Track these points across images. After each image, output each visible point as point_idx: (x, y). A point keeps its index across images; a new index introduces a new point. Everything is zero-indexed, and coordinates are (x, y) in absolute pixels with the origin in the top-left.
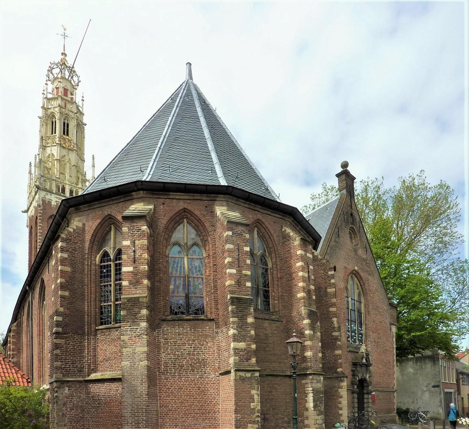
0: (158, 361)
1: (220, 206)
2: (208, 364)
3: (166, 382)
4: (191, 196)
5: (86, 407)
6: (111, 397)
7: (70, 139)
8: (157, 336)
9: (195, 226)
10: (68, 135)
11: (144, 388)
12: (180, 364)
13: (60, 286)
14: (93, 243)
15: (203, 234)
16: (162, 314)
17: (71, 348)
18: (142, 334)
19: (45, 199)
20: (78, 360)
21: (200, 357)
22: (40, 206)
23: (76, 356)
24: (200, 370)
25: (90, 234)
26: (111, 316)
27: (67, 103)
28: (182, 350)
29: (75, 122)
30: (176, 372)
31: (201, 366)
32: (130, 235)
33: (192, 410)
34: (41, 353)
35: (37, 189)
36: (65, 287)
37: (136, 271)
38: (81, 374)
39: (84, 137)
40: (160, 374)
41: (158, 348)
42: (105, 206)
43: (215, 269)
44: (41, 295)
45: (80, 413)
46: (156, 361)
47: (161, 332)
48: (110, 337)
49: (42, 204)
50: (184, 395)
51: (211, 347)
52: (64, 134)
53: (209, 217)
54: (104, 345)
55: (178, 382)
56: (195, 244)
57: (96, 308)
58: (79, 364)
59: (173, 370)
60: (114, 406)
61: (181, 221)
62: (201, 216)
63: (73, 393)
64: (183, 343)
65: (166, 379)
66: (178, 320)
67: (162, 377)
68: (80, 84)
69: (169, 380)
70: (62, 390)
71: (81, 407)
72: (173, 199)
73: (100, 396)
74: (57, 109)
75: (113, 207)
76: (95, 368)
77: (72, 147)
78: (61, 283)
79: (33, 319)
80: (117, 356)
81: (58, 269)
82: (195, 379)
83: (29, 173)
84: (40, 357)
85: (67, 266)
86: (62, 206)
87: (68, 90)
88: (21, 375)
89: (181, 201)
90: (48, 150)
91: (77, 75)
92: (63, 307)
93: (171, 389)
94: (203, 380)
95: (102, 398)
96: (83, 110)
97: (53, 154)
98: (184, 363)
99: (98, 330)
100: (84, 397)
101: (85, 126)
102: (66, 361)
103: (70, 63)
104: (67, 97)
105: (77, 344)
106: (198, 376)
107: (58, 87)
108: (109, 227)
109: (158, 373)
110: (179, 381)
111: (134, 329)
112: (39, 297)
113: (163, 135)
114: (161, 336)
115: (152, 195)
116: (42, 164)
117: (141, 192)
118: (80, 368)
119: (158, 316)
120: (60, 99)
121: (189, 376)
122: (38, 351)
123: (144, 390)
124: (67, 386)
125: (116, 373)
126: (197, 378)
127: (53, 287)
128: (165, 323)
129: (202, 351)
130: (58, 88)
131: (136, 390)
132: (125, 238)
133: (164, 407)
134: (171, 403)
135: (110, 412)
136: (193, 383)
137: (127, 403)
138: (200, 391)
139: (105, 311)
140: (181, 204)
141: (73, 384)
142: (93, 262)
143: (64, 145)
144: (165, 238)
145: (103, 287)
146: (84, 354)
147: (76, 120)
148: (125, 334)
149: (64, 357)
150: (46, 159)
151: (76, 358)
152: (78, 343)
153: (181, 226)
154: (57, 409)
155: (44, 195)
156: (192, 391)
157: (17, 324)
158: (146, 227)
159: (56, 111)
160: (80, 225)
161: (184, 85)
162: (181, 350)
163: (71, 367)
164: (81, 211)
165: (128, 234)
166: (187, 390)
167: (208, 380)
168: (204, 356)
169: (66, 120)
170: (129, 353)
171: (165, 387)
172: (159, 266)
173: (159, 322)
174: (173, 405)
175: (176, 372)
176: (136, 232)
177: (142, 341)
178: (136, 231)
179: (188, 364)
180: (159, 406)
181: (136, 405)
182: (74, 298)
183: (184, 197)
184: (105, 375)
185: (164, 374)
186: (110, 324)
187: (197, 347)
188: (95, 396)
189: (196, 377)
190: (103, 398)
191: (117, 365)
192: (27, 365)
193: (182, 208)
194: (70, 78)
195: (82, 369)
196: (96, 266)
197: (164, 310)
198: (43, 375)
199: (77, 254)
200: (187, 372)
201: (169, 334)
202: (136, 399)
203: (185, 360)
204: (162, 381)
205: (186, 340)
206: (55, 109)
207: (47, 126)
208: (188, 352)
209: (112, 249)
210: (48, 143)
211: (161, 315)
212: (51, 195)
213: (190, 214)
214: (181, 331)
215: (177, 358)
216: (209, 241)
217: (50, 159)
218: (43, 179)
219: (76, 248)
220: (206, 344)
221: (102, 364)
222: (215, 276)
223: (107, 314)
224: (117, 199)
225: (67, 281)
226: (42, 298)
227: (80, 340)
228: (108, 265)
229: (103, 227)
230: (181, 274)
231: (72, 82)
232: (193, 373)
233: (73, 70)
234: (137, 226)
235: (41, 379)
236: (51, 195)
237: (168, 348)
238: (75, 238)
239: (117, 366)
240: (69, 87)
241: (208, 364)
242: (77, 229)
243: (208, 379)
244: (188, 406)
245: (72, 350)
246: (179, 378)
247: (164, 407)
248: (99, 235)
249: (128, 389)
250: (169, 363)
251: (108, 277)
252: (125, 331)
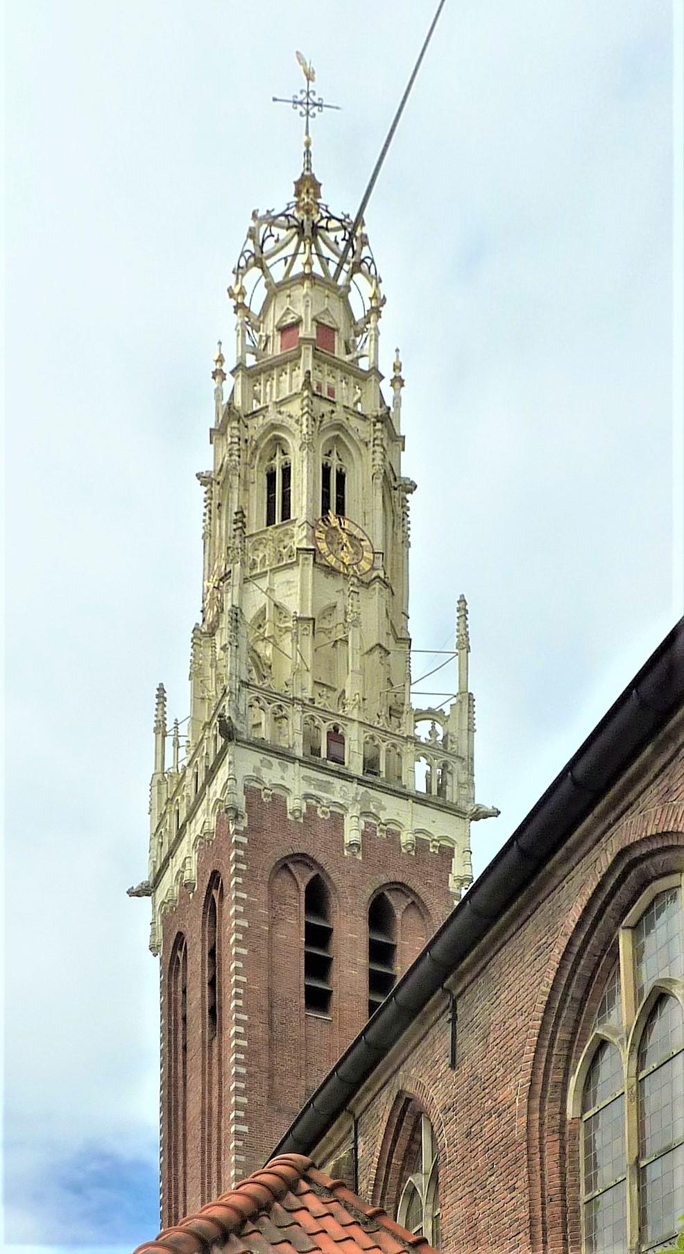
19: (258, 786)
22: (236, 817)
35: (221, 741)
49: (244, 805)
74: (295, 408)
83: (156, 730)
87: (333, 330)
101: (408, 496)
143: (332, 560)
155: (257, 770)
159: (290, 416)
206: (282, 409)
212: (284, 768)
233: (358, 234)
236: (284, 768)
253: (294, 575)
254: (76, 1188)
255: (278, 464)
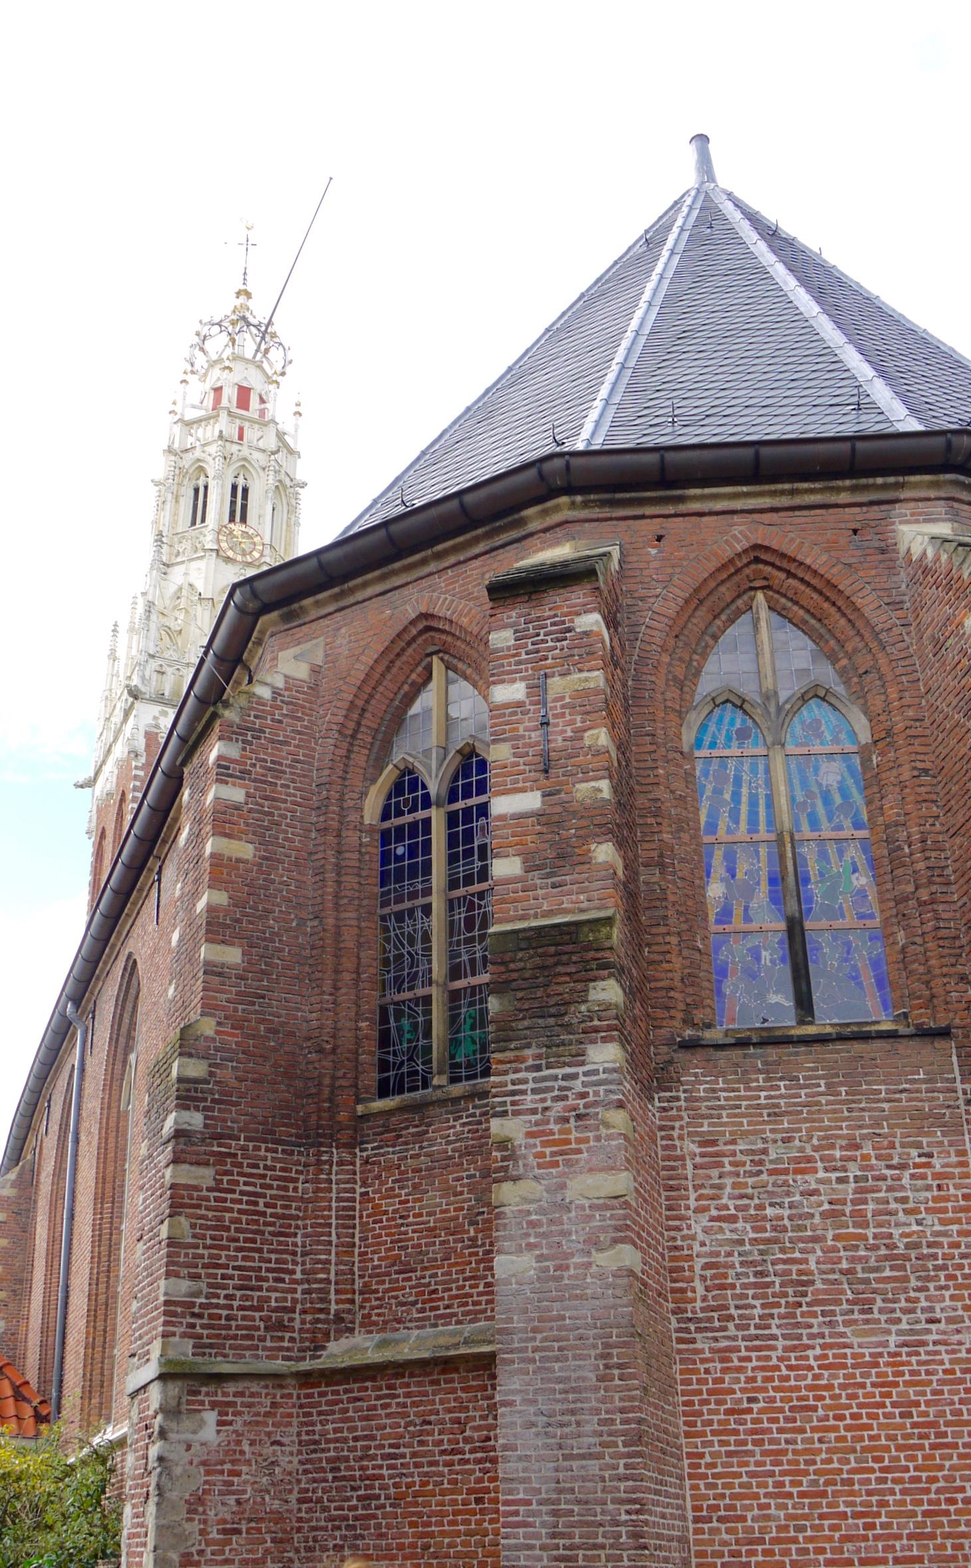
0: (673, 1259)
1: (917, 522)
2: (944, 1267)
3: (725, 1370)
4: (782, 493)
5: (300, 1520)
6: (431, 1464)
7: (251, 532)
8: (661, 1128)
9: (807, 617)
10: (244, 519)
11: (621, 1399)
12: (788, 1273)
13: (208, 923)
14: (353, 737)
15: (849, 647)
16: (680, 1015)
17: (240, 1211)
18: (595, 1104)
20: (268, 1270)
21: (896, 1232)
22: (137, 756)
23: (260, 1250)
24: (903, 1304)
25: (339, 704)
26: (428, 1049)
27: (245, 429)
28: (797, 1198)
29: (271, 477)
30: (772, 1316)
31: (906, 1279)
32: (524, 657)
33: (877, 1538)
34: (103, 1279)
35: (131, 699)
36: (228, 927)
37: (558, 809)
38: (282, 1339)
39: (297, 524)
40: (687, 1330)
41: (671, 1188)
42: (407, 584)
43: (928, 789)
44: (119, 1030)
45: (267, 1551)
46: (663, 1256)
47: (682, 1103)
48: (421, 1148)
49: (143, 747)
50: (828, 1450)
51: (950, 1176)
52: (232, 519)
53: (873, 572)
54: (392, 1189)
55: (785, 1372)
56: (815, 694)
57: (358, 1017)
58: (276, 1290)
59: (757, 1303)
60: (442, 1514)
61: (740, 602)
62: (834, 570)
63: (239, 1443)
64: (797, 1160)
65: (724, 1355)
66: (762, 1044)
67: (699, 1346)
68: (288, 369)
69: (736, 1363)
70: (187, 1423)
71: (278, 1518)
72: (701, 514)
73: (374, 1458)
74: (212, 449)
75: (440, 581)
76: (349, 1311)
77: (256, 555)
78: (210, 909)
79: (83, 1137)
80: (455, 1241)
81: (200, 856)
82: (881, 1355)
84: (97, 1295)
85: (240, 839)
86: (232, 610)
88: (12, 1384)
89: (736, 518)
90: (177, 576)
91: (280, 344)
92: (213, 1015)
93: (750, 1411)
94: (923, 1357)
95: (381, 1467)
96: (296, 442)
97: (191, 585)
98: (813, 1266)
99: (365, 1117)
100: (289, 1468)
102: (215, 1276)
103: (259, 311)
104: (247, 409)
105: (270, 1187)
106: (893, 1339)
107: (219, 385)
108: (420, 669)
109: (674, 1324)
110: (790, 1368)
111: (556, 1078)
112: (111, 1039)
113: (614, 362)
114: (681, 1128)
115: (607, 510)
116: (154, 617)
117: (564, 500)
118: (276, 1310)
119: (661, 1027)
120: (223, 416)
121: (843, 1335)
122: (92, 1269)
123: (622, 1411)
124: (214, 1405)
125: (453, 1334)
126: (892, 1349)
127: (175, 937)
128: (697, 1057)
129: (904, 1200)
130: (221, 388)
131: (573, 1412)
132: (504, 673)
133: (720, 1519)
134: (756, 1496)
135: (426, 1547)
136: (868, 1375)
137: (526, 1491)
138: (915, 1425)
139: (399, 1029)
140: (736, 531)
141: (242, 1394)
142: (353, 817)
143: (230, 554)
144: (675, 677)
145: (391, 924)
146: (299, 1240)
147: (272, 473)
148: (509, 1108)
149: (206, 1252)
150: (167, 602)
151: (262, 1260)
152: (275, 1183)
153: (739, 629)
154: (159, 1528)
155: (155, 718)
156: (869, 1427)
157: (20, 1175)
158: (595, 617)
160: (301, 671)
161: (689, 201)
162: (788, 1194)
163: (236, 1304)
164: (307, 620)
165: (514, 656)
166: (841, 1418)
167: (952, 1362)
168: (919, 1223)
169: (241, 477)
170: (532, 1207)
171: (718, 1403)
172: (651, 796)
173: (667, 1058)
174: (768, 1506)
175: (772, 1316)
176: (550, 644)
177: (598, 1138)
178: (549, 638)
179: (833, 1271)
180: (690, 1515)
181: (579, 1502)
182: (263, 972)
183: (752, 503)
184: (397, 1342)
185: (706, 1329)
186: (426, 1085)
187: (876, 1178)
188: (347, 1459)
189: (885, 1344)
190: (390, 1467)
191: (458, 1288)
192: (43, 1346)
193: (746, 544)
194: (259, 355)
195: (286, 1317)
196: (361, 831)
197: (689, 1000)
198: (102, 1382)
199: (283, 786)
200: (833, 1313)
201: (724, 1113)
202: (575, 1464)
203: (817, 1247)
204: (702, 1367)
205: (815, 1142)
207: (177, 501)
208: (826, 1206)
209: (434, 755)
210: (178, 554)
211: (677, 1023)
213: (780, 569)
214: (781, 1096)
215: (776, 1241)
216: (885, 669)
217: (183, 603)
218: (154, 664)
219: (281, 764)
220: (923, 1160)
221: (381, 1287)
222: (931, 821)
223: (409, 1041)
224: (455, 549)
225: (236, 903)
226: (122, 1040)
227: (282, 1169)
228: (413, 825)
229: (394, 670)
230: (758, 832)
231: (265, 365)
232: (867, 1322)
234: (555, 616)
235: (95, 1401)
237: (720, 1187)
238: (280, 722)
239: (457, 1297)
240: (254, 380)
241: (944, 1267)
242: (286, 689)
243: (954, 1352)
244: (857, 1515)
245: (244, 1218)
246: (794, 1349)
247: (720, 1519)
248: (378, 705)
249: (532, 1409)
250: (733, 1266)
251: (413, 875)
252: (513, 1093)
253: (201, 564)
254: (479, 670)
255: (201, 483)
